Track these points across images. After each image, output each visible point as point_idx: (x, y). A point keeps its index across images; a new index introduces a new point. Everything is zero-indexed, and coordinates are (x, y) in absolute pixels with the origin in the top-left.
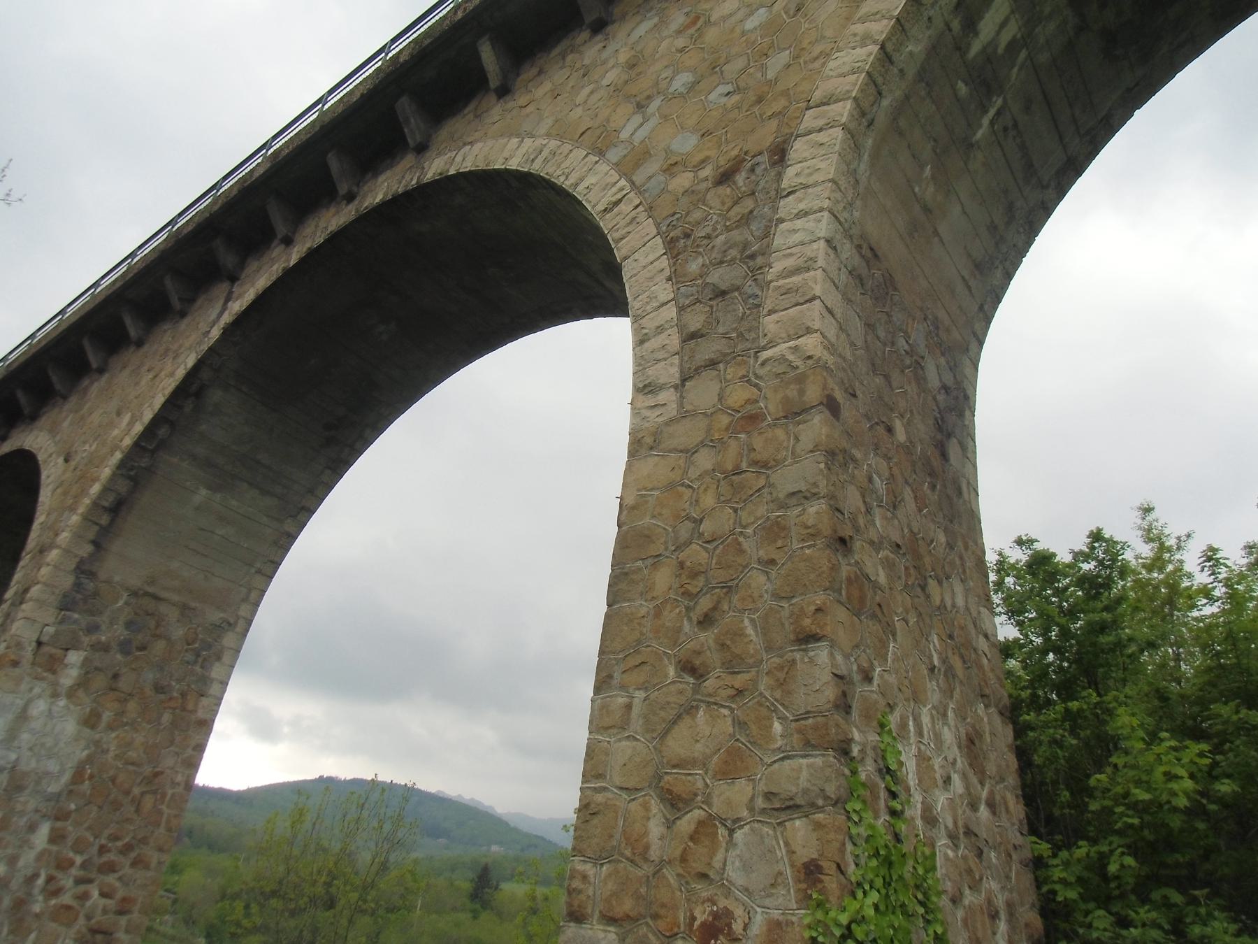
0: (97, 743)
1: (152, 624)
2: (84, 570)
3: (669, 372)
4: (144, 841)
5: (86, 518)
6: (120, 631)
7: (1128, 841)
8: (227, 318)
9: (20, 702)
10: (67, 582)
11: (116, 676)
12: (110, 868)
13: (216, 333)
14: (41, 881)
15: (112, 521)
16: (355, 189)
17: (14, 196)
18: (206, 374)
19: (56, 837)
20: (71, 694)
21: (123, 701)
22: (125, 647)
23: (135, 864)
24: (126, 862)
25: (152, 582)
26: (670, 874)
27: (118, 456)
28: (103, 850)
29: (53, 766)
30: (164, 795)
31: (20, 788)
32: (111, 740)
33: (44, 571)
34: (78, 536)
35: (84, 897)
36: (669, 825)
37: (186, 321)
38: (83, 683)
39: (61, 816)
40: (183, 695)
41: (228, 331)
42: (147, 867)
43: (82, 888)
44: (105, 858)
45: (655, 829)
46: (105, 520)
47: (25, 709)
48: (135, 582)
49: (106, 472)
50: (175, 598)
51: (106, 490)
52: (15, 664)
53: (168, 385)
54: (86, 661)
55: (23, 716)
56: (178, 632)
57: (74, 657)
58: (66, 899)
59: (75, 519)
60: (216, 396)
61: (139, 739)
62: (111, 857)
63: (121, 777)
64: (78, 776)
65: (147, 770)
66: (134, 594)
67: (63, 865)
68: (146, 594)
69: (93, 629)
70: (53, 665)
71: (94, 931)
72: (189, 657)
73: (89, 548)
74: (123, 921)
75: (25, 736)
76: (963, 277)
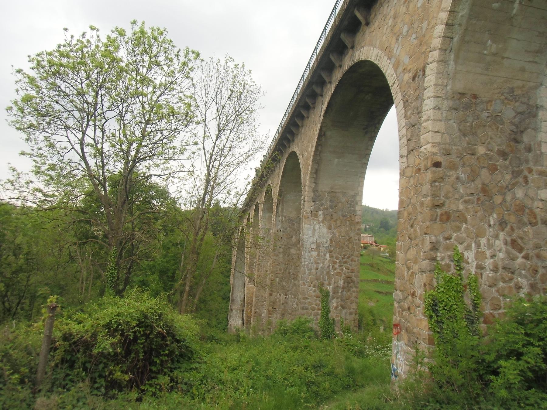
0: (333, 233)
1: (336, 200)
2: (315, 190)
3: (405, 152)
4: (352, 255)
5: (310, 177)
6: (329, 203)
7: (484, 281)
8: (323, 112)
9: (312, 226)
10: (312, 194)
11: (332, 215)
12: (346, 262)
13: (322, 117)
14: (331, 267)
15: (317, 176)
16: (341, 63)
17: (265, 93)
18: (324, 129)
19: (331, 256)
20: (323, 222)
21: (335, 221)
22: (331, 207)
23: (352, 261)
24: (349, 260)
25: (332, 188)
26: (408, 283)
27: (312, 158)
28: (343, 258)
29: (325, 240)
30: (354, 243)
31: (319, 246)
32: (336, 231)
33: (306, 193)
34: (310, 182)
35: (342, 270)
36: (408, 273)
37: (316, 109)
38: (325, 219)
39: (330, 251)
40: (350, 216)
41: (324, 116)
42: (355, 261)
43: (341, 268)
44: (344, 260)
45: (406, 273)
46: (315, 176)
47: (314, 228)
48: (328, 190)
49: (311, 163)
50: (340, 191)
51: (312, 168)
52: (308, 217)
53: (316, 134)
54: (323, 213)
55: (314, 230)
56: (344, 200)
57: (320, 213)
58: (338, 270)
59: (308, 177)
60: (329, 133)
61: (343, 230)
62: (345, 260)
63: (341, 240)
64: (331, 242)
65: (348, 238)
66: (329, 193)
67: (335, 263)
68: (332, 192)
69: (322, 204)
70: (316, 216)
71: (347, 277)
72: (349, 206)
73: (314, 184)
74: (353, 274)
75: (316, 234)
76: (529, 62)
